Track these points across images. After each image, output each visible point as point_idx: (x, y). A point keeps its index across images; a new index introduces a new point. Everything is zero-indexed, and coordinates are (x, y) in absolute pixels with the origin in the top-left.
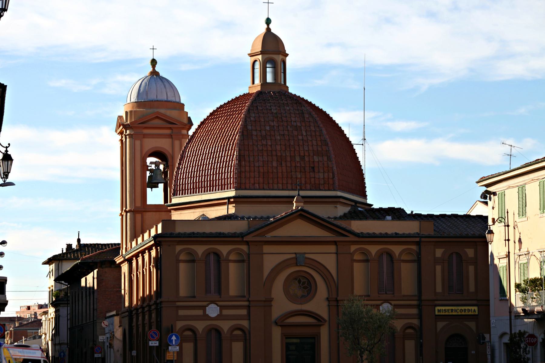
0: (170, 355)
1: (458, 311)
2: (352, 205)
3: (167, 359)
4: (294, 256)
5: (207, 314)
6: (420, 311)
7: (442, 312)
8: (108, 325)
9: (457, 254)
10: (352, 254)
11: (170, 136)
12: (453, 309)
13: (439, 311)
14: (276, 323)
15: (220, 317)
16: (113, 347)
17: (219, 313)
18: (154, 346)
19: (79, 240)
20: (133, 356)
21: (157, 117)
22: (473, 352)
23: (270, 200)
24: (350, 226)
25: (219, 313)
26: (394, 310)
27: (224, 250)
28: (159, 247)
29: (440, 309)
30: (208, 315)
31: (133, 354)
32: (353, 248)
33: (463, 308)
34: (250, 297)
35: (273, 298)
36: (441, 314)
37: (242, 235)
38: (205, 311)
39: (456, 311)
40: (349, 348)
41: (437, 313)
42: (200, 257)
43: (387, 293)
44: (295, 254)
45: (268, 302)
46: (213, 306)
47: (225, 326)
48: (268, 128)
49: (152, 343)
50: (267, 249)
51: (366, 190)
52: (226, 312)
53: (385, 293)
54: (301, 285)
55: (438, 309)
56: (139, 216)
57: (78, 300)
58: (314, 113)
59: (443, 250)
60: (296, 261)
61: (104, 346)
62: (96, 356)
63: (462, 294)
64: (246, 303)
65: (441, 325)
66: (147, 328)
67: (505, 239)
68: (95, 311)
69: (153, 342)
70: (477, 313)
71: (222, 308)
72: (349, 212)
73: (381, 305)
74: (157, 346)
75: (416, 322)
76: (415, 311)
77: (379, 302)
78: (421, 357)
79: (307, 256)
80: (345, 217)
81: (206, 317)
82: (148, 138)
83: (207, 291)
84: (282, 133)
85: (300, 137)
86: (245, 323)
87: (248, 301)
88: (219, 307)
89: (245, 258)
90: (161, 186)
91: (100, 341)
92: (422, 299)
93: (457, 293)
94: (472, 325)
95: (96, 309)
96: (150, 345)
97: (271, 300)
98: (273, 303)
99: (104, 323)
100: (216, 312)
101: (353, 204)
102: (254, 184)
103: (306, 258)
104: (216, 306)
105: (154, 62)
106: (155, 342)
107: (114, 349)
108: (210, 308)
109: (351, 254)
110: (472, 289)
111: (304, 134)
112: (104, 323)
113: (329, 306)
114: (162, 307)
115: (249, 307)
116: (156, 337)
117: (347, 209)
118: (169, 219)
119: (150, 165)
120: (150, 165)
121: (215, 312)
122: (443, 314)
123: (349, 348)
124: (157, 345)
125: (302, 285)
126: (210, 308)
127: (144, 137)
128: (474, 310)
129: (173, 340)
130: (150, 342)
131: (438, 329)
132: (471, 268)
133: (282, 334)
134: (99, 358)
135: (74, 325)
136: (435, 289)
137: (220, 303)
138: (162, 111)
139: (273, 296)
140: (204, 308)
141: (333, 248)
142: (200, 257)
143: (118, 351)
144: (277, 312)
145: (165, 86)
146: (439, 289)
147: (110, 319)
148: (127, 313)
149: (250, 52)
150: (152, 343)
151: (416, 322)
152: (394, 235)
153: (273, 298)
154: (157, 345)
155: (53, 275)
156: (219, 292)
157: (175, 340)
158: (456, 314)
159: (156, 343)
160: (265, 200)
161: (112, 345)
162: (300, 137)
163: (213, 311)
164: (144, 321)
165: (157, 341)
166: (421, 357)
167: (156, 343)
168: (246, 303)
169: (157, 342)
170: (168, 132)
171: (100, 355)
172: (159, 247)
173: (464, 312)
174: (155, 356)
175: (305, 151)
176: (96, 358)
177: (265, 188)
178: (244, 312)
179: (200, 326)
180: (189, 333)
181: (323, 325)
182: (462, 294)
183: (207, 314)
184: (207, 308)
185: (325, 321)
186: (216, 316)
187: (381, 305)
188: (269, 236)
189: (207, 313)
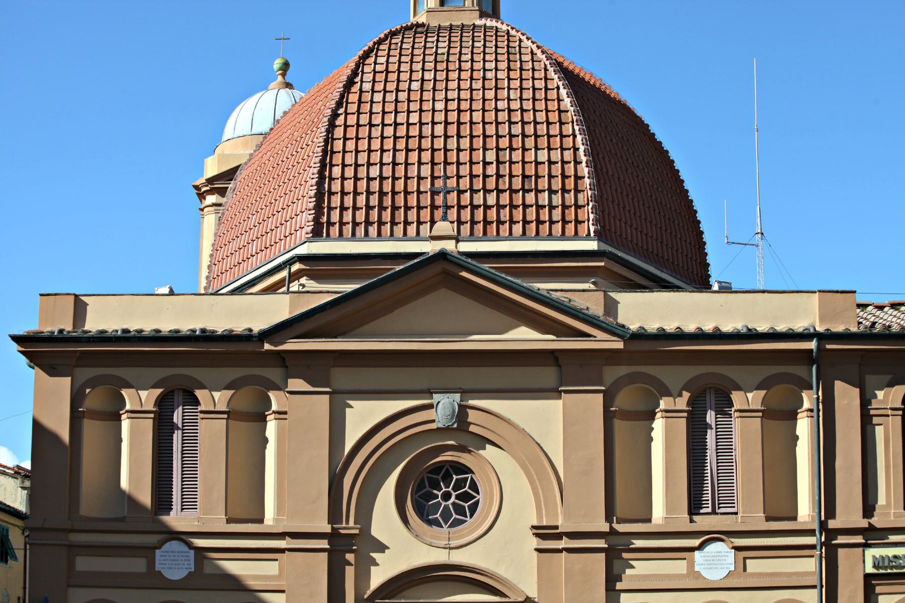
5: (156, 569)
17: (193, 570)
25: (193, 570)
30: (160, 572)
38: (691, 564)
40: (701, 580)
51: (651, 132)
58: (587, 181)
73: (159, 548)
88: (192, 552)
100: (186, 566)
104: (186, 548)
108: (166, 552)
118: (332, 395)
121: (181, 566)
123: (701, 580)
125: (455, 489)
126: (166, 552)
129: (888, 538)
155: (725, 560)
175: (703, 522)
183: (156, 569)
184: (157, 551)
186: (187, 576)
187: (159, 547)
189: (158, 567)
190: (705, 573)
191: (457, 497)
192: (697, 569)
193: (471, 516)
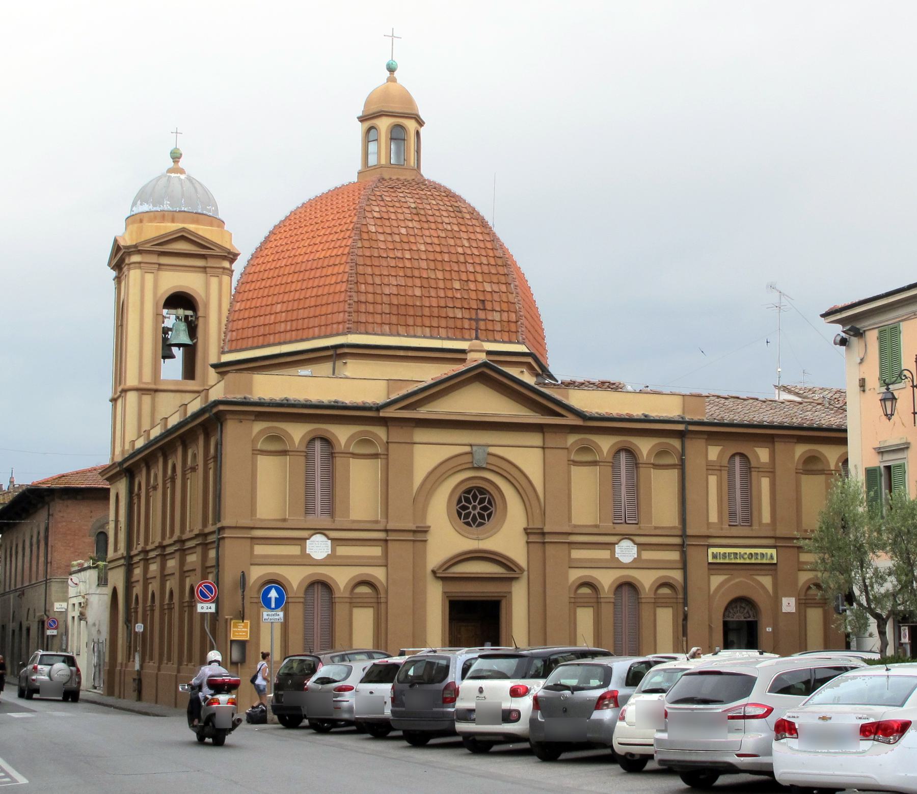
0: (238, 632)
1: (746, 556)
3: (233, 638)
4: (468, 449)
6: (684, 555)
7: (720, 558)
8: (78, 582)
9: (742, 455)
12: (736, 554)
13: (714, 556)
15: (331, 561)
16: (86, 618)
18: (207, 613)
19: (11, 482)
20: (137, 632)
21: (183, 238)
22: (769, 629)
23: (410, 354)
24: (567, 398)
26: (333, 549)
27: (342, 434)
29: (717, 553)
31: (137, 630)
33: (753, 551)
34: (387, 522)
35: (429, 527)
36: (718, 561)
37: (378, 408)
38: (304, 549)
39: (742, 556)
41: (710, 560)
42: (297, 445)
43: (628, 522)
44: (471, 445)
45: (420, 533)
46: (319, 538)
47: (341, 578)
49: (202, 608)
50: (420, 435)
52: (342, 551)
53: (623, 521)
54: (471, 506)
55: (713, 553)
56: (147, 399)
57: (17, 553)
59: (720, 448)
61: (66, 617)
62: (49, 632)
63: (751, 526)
64: (381, 535)
65: (716, 580)
67: (913, 411)
68: (49, 565)
69: (205, 605)
70: (775, 561)
73: (617, 544)
74: (211, 613)
75: (676, 576)
76: (674, 556)
78: (685, 639)
79: (492, 450)
81: (306, 560)
82: (166, 270)
83: (309, 510)
86: (379, 574)
87: (386, 531)
91: (55, 610)
92: (688, 534)
93: (742, 524)
94: (766, 581)
95: (51, 563)
96: (199, 610)
97: (425, 531)
99: (71, 579)
100: (326, 550)
103: (489, 454)
105: (176, 157)
106: (209, 605)
107: (87, 622)
109: (567, 448)
110: (766, 518)
112: (71, 579)
113: (528, 543)
114: (223, 538)
116: (210, 596)
119: (167, 316)
120: (167, 316)
122: (722, 561)
124: (213, 610)
125: (479, 504)
127: (159, 269)
128: (772, 557)
129: (270, 598)
130: (199, 606)
131: (712, 592)
132: (765, 483)
133: (444, 593)
134: (53, 636)
135: (7, 590)
136: (708, 520)
138: (191, 227)
139: (429, 522)
142: (297, 445)
143: (94, 625)
146: (713, 517)
147: (79, 574)
148: (122, 562)
150: (202, 608)
151: (676, 576)
152: (643, 417)
153: (429, 527)
154: (213, 610)
156: (330, 510)
157: (276, 598)
158: (742, 561)
159: (210, 608)
160: (402, 353)
161: (84, 615)
163: (319, 547)
164: (184, 566)
165: (213, 602)
166: (685, 639)
167: (210, 608)
168: (381, 535)
169: (213, 606)
170: (200, 263)
171: (55, 632)
173: (755, 559)
174: (209, 633)
176: (48, 636)
177: (400, 332)
178: (377, 551)
179: (606, 579)
180: (585, 590)
181: (517, 578)
182: (751, 526)
185: (521, 570)
190: (621, 559)
191: (481, 509)
192: (617, 556)
193: (488, 521)
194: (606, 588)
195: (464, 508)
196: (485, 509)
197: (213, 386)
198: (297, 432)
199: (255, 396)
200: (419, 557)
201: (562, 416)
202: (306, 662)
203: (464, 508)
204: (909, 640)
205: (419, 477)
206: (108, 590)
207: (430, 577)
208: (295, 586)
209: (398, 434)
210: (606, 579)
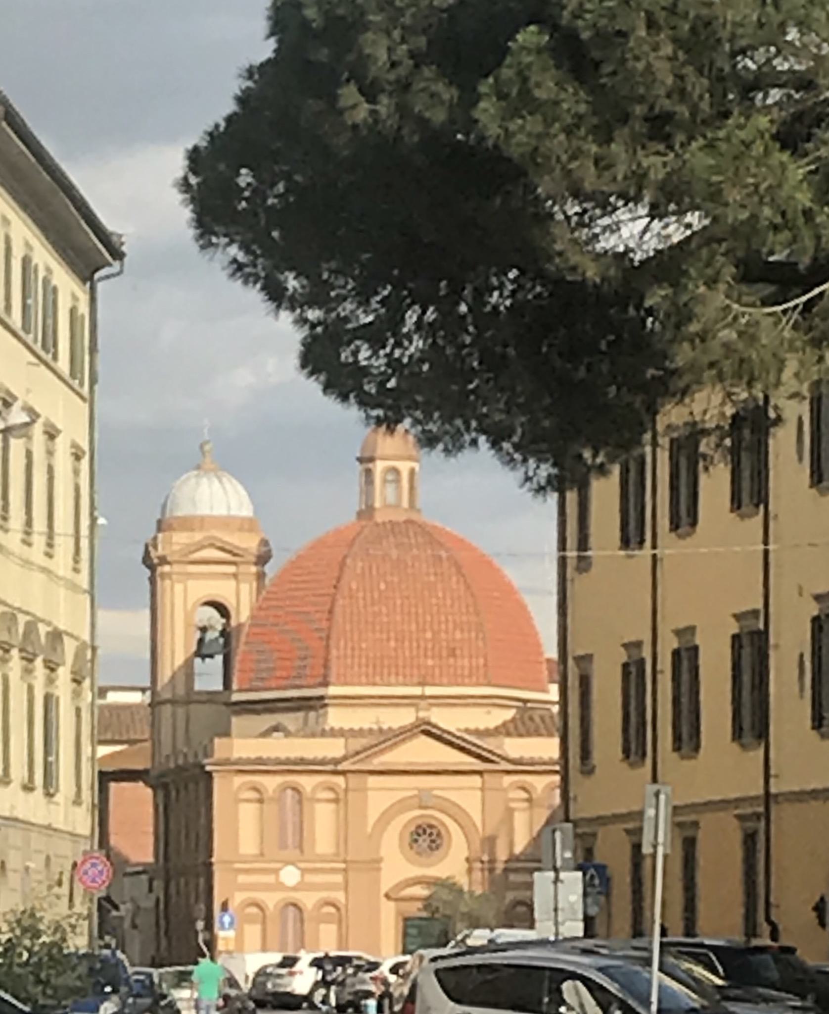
2: (517, 707)
4: (416, 792)
10: (505, 790)
11: (235, 576)
14: (387, 896)
21: (212, 545)
26: (302, 876)
27: (307, 783)
28: (373, 391)
32: (508, 780)
37: (336, 762)
44: (419, 790)
45: (375, 864)
46: (290, 869)
47: (308, 900)
48: (383, 586)
52: (310, 878)
56: (181, 711)
60: (422, 801)
64: (343, 866)
66: (192, 900)
71: (304, 871)
72: (513, 720)
77: (278, 865)
80: (505, 730)
81: (280, 886)
83: (283, 846)
84: (406, 593)
85: (434, 601)
86: (339, 896)
87: (345, 862)
89: (342, 796)
90: (219, 658)
97: (379, 860)
98: (383, 865)
101: (520, 704)
102: (360, 676)
111: (440, 594)
115: (345, 870)
117: (509, 714)
133: (398, 913)
137: (302, 865)
139: (383, 853)
140: (276, 871)
141: (476, 780)
144: (388, 880)
145: (224, 488)
149: (358, 455)
162: (434, 601)
163: (290, 875)
168: (343, 866)
170: (231, 569)
172: (373, 391)
178: (339, 878)
179: (271, 900)
180: (254, 910)
188: (377, 763)
194: (271, 791)
195: (416, 841)
196: (433, 841)
197: (354, 539)
198: (271, 783)
199: (236, 755)
200: (377, 882)
201: (492, 762)
202: (669, 851)
203: (416, 841)
204: (366, 1006)
205: (373, 815)
206: (153, 897)
207: (384, 900)
208: (271, 791)
209: (353, 779)
210: (271, 900)
